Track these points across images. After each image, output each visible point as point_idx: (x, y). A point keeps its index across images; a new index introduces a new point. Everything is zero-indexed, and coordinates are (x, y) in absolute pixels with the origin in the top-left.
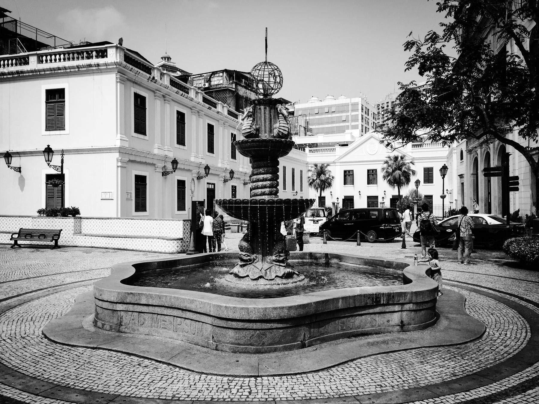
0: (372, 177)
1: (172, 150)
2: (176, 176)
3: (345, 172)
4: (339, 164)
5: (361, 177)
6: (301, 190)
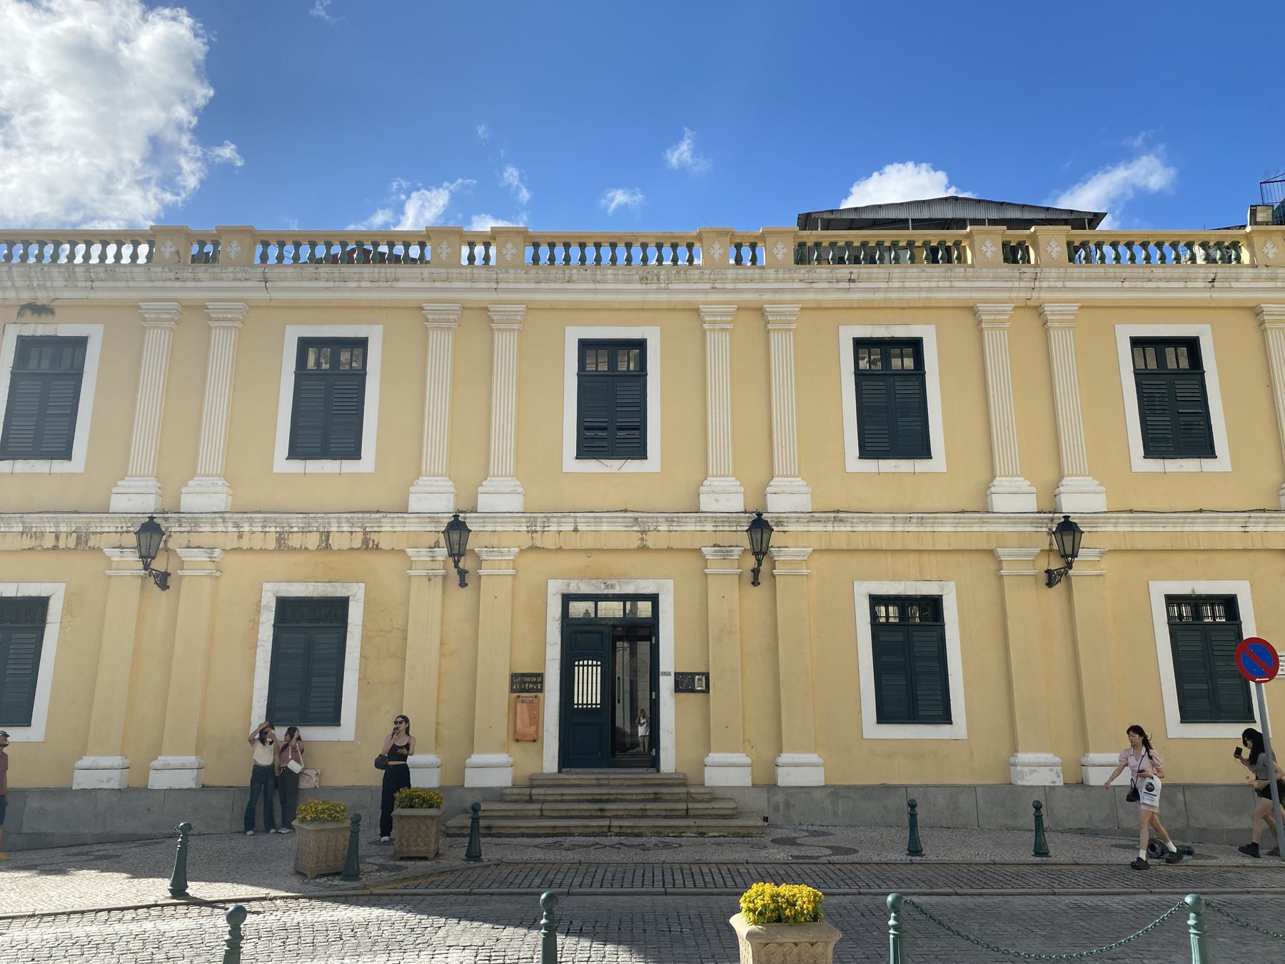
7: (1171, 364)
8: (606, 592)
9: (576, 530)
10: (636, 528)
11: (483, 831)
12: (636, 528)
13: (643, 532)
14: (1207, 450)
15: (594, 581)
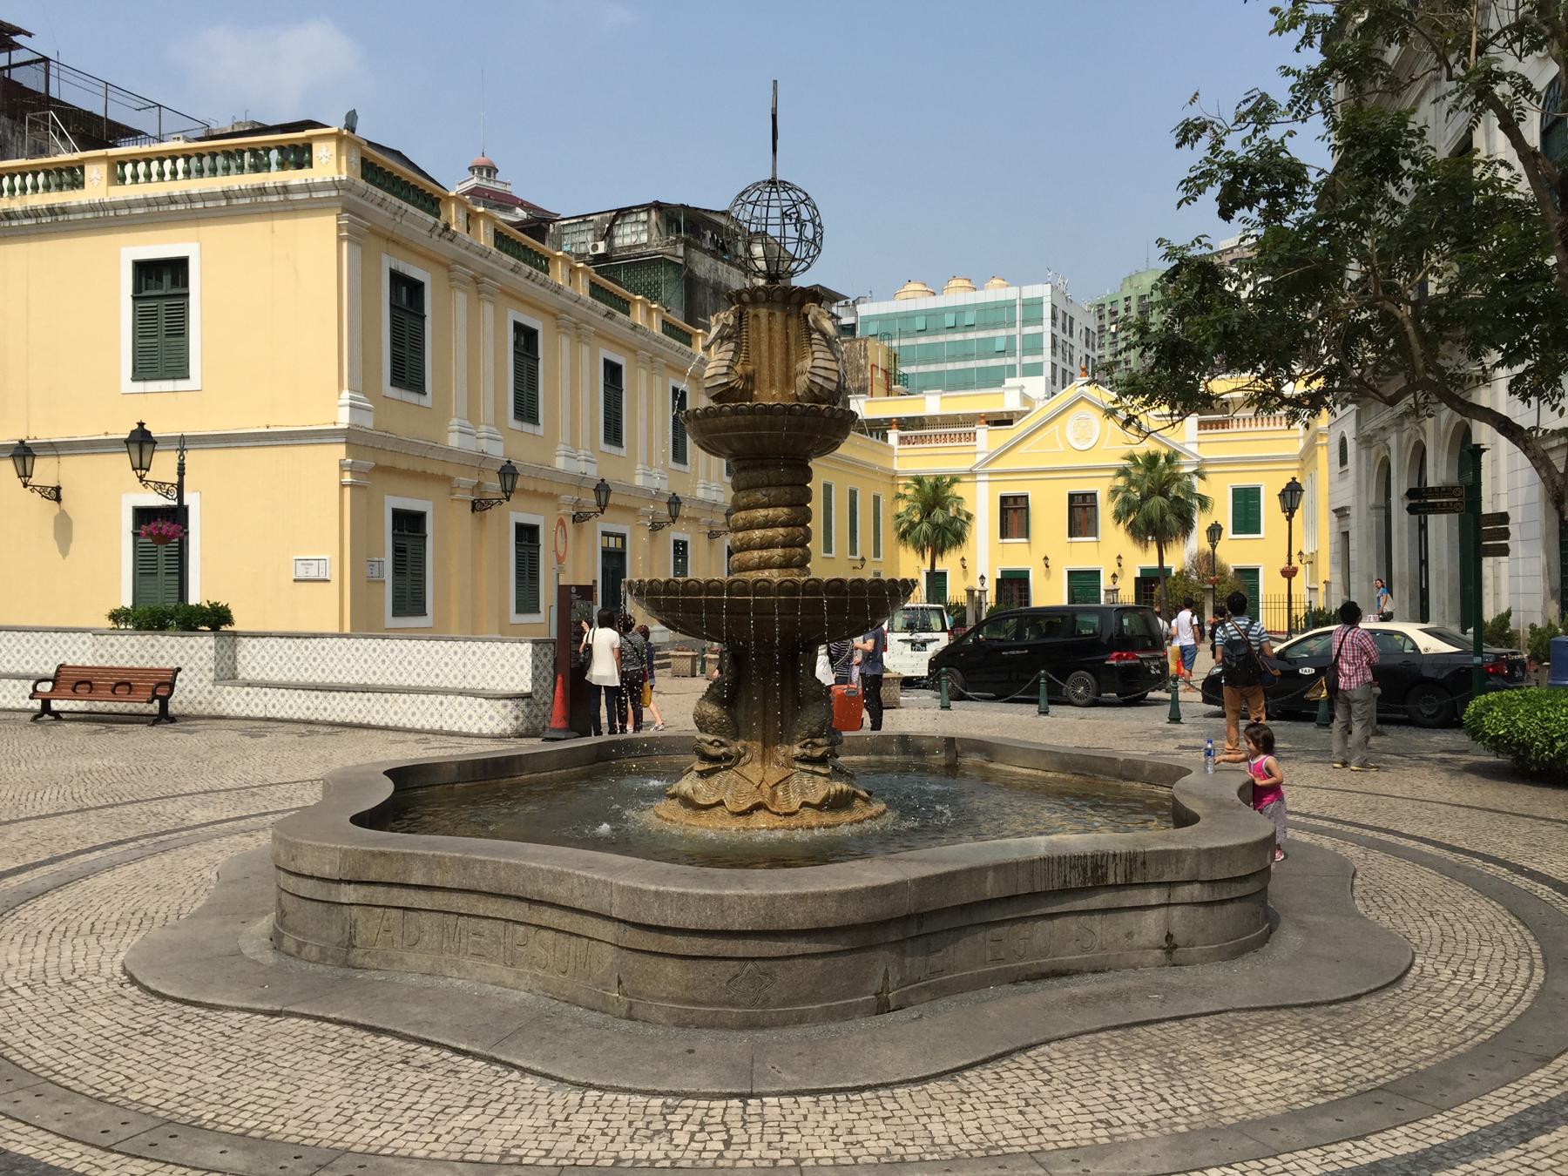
0: (1081, 515)
2: (512, 514)
3: (1004, 499)
4: (986, 478)
5: (1049, 513)
6: (877, 554)
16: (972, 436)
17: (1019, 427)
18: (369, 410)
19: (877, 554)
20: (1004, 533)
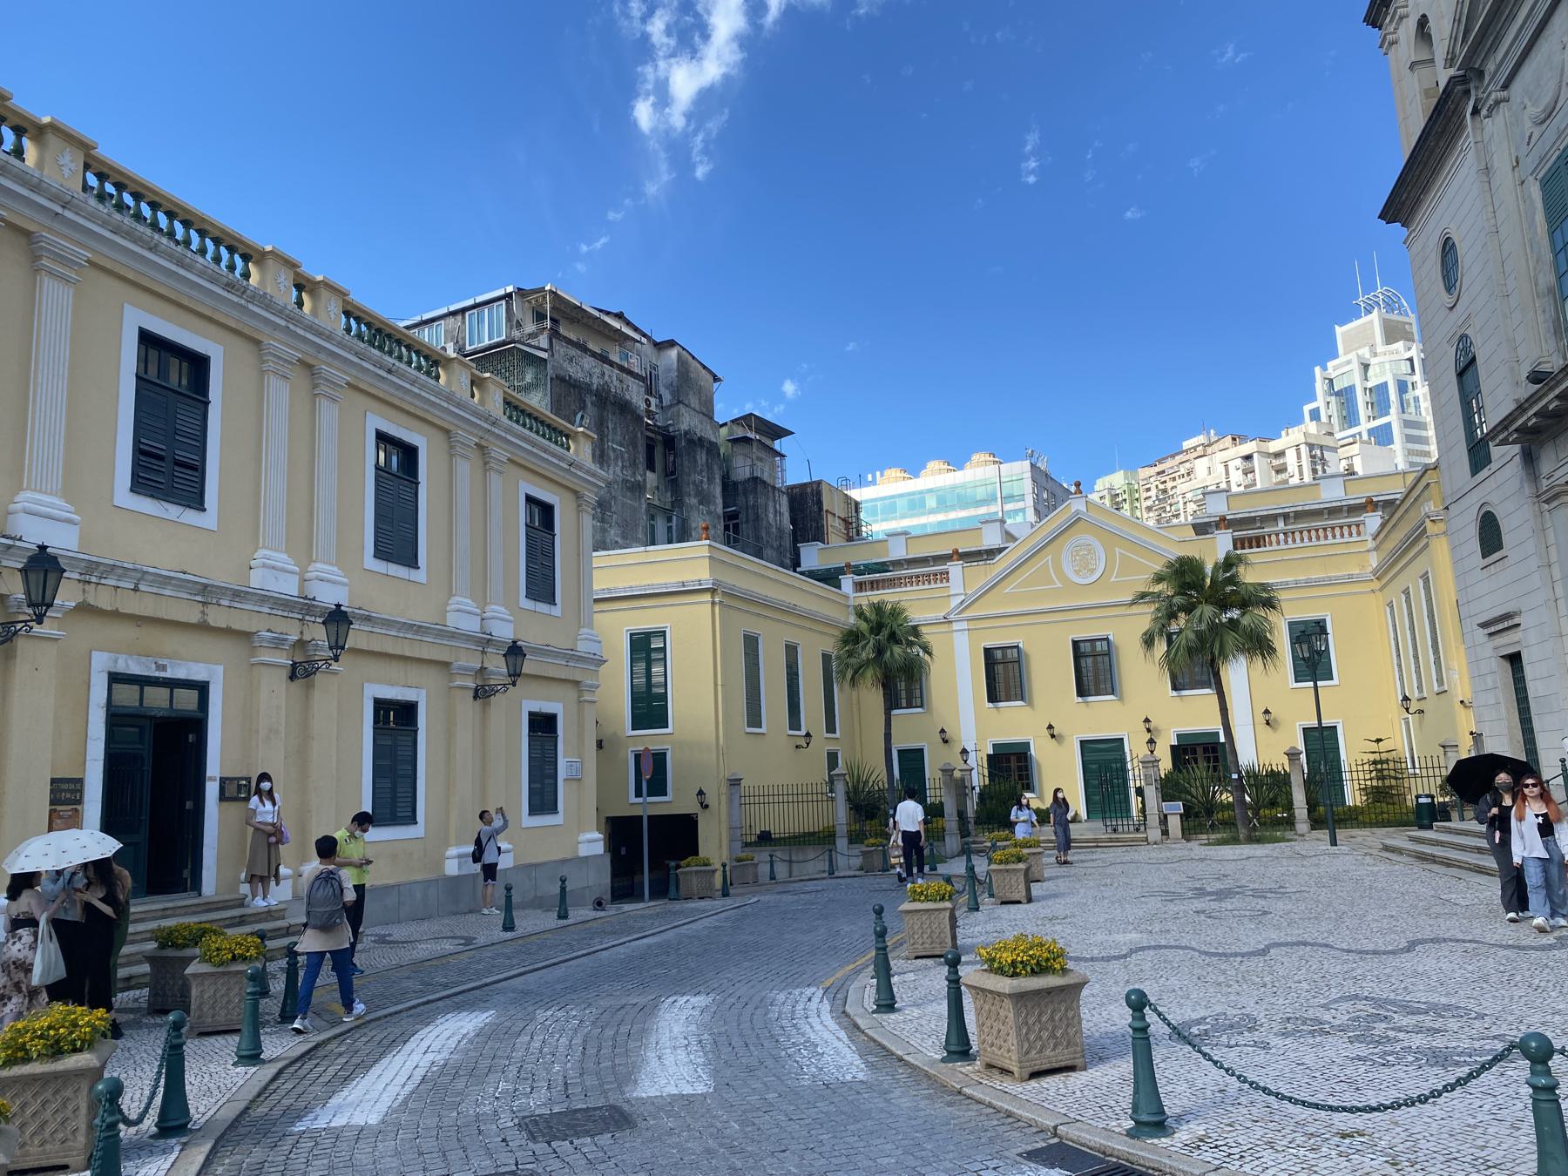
0: (1094, 670)
1: (512, 616)
2: (524, 703)
3: (988, 652)
4: (964, 625)
5: (1051, 671)
6: (831, 728)
7: (173, 381)
8: (157, 674)
9: (136, 589)
10: (199, 598)
11: (120, 985)
12: (199, 598)
13: (204, 603)
14: (196, 501)
15: (144, 659)
16: (945, 576)
17: (1001, 564)
18: (344, 584)
19: (831, 728)
20: (993, 697)
